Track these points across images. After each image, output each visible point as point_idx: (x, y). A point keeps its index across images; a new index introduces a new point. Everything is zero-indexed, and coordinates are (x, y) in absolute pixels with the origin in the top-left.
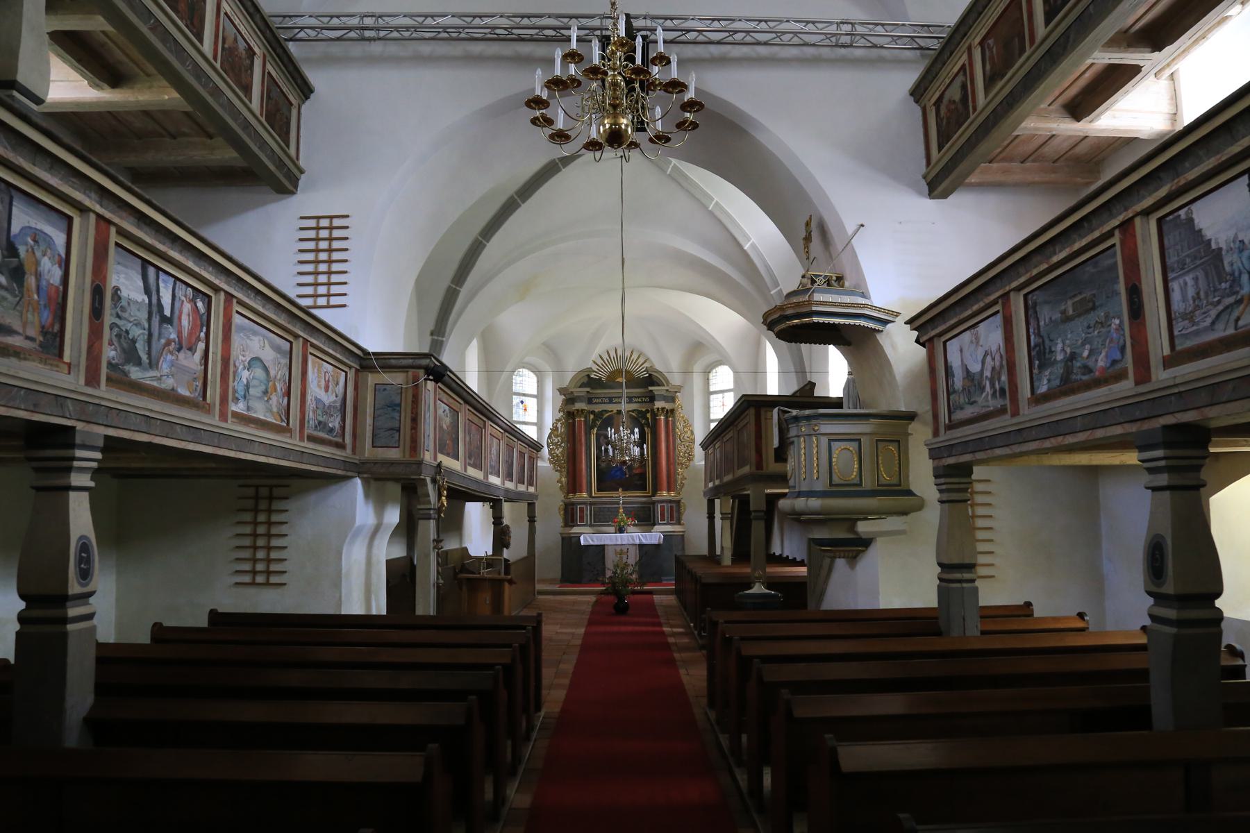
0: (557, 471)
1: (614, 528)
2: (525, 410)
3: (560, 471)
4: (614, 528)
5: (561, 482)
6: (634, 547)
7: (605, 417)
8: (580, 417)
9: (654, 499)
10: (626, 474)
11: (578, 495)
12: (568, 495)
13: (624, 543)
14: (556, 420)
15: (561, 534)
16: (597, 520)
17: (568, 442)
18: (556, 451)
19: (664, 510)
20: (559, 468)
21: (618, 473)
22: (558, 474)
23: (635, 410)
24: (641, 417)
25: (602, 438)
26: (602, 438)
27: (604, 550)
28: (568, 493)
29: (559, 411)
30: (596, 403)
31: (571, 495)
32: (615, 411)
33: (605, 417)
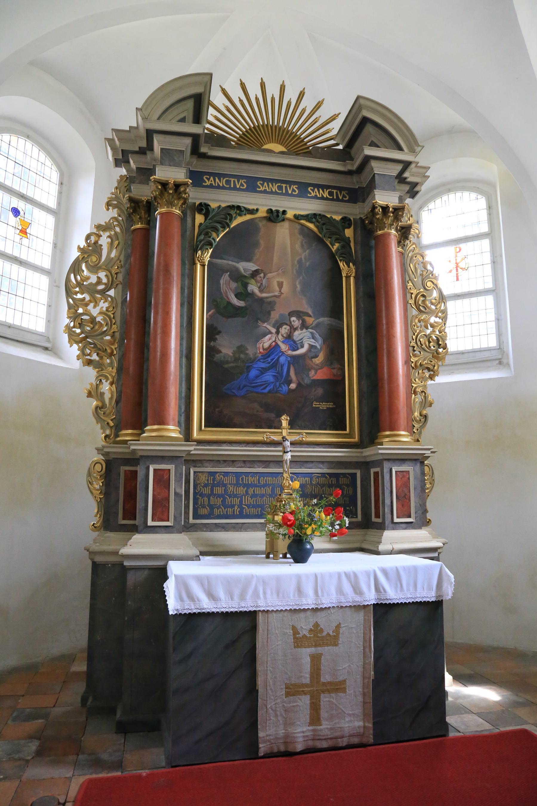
0: (89, 363)
1: (261, 535)
2: (24, 232)
3: (98, 366)
4: (261, 535)
5: (100, 396)
6: (361, 616)
7: (234, 224)
8: (170, 204)
9: (369, 452)
10: (289, 382)
11: (151, 431)
12: (117, 436)
13: (326, 602)
14: (99, 227)
15: (92, 553)
16: (204, 511)
17: (127, 285)
18: (91, 307)
19: (407, 484)
20: (95, 357)
21: (269, 377)
22: (91, 373)
23: (315, 215)
24: (331, 234)
25: (226, 277)
26: (226, 277)
27: (253, 629)
28: (118, 428)
29: (108, 204)
30: (211, 186)
31: (127, 434)
32: (262, 213)
33: (234, 224)
